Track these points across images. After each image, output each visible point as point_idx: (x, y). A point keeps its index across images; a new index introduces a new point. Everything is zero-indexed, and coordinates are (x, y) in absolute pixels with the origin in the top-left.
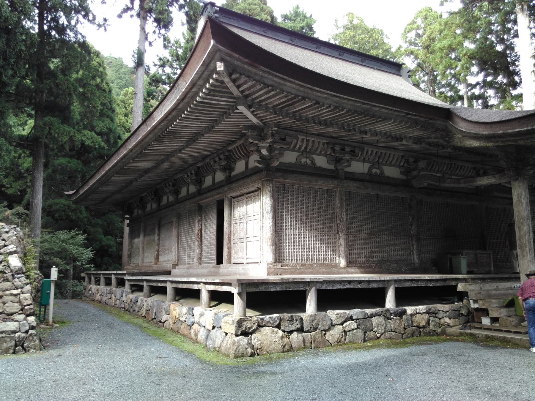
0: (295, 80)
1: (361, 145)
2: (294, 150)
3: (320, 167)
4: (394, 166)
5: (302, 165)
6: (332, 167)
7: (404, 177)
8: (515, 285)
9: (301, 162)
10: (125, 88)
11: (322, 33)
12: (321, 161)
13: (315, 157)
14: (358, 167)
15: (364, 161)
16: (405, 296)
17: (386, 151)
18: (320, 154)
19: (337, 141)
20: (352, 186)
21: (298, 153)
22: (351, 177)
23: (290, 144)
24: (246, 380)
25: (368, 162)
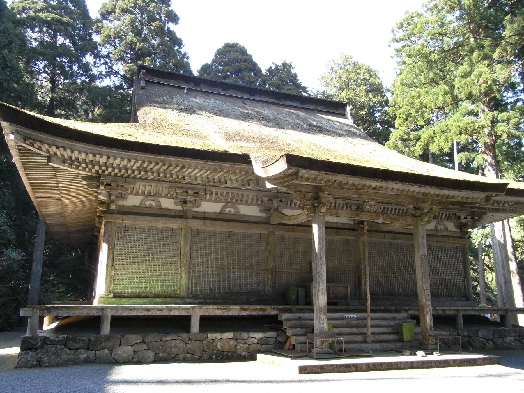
0: (16, 171)
1: (204, 187)
2: (137, 194)
3: (166, 208)
4: (251, 204)
5: (146, 207)
6: (180, 208)
7: (263, 215)
8: (347, 316)
9: (145, 205)
10: (469, 135)
11: (313, 81)
12: (168, 203)
13: (161, 199)
14: (211, 207)
15: (216, 201)
16: (209, 323)
17: (243, 193)
18: (166, 197)
19: (179, 185)
20: (197, 224)
21: (142, 197)
22: (204, 217)
23: (127, 189)
24: (11, 60)
25: (221, 201)
